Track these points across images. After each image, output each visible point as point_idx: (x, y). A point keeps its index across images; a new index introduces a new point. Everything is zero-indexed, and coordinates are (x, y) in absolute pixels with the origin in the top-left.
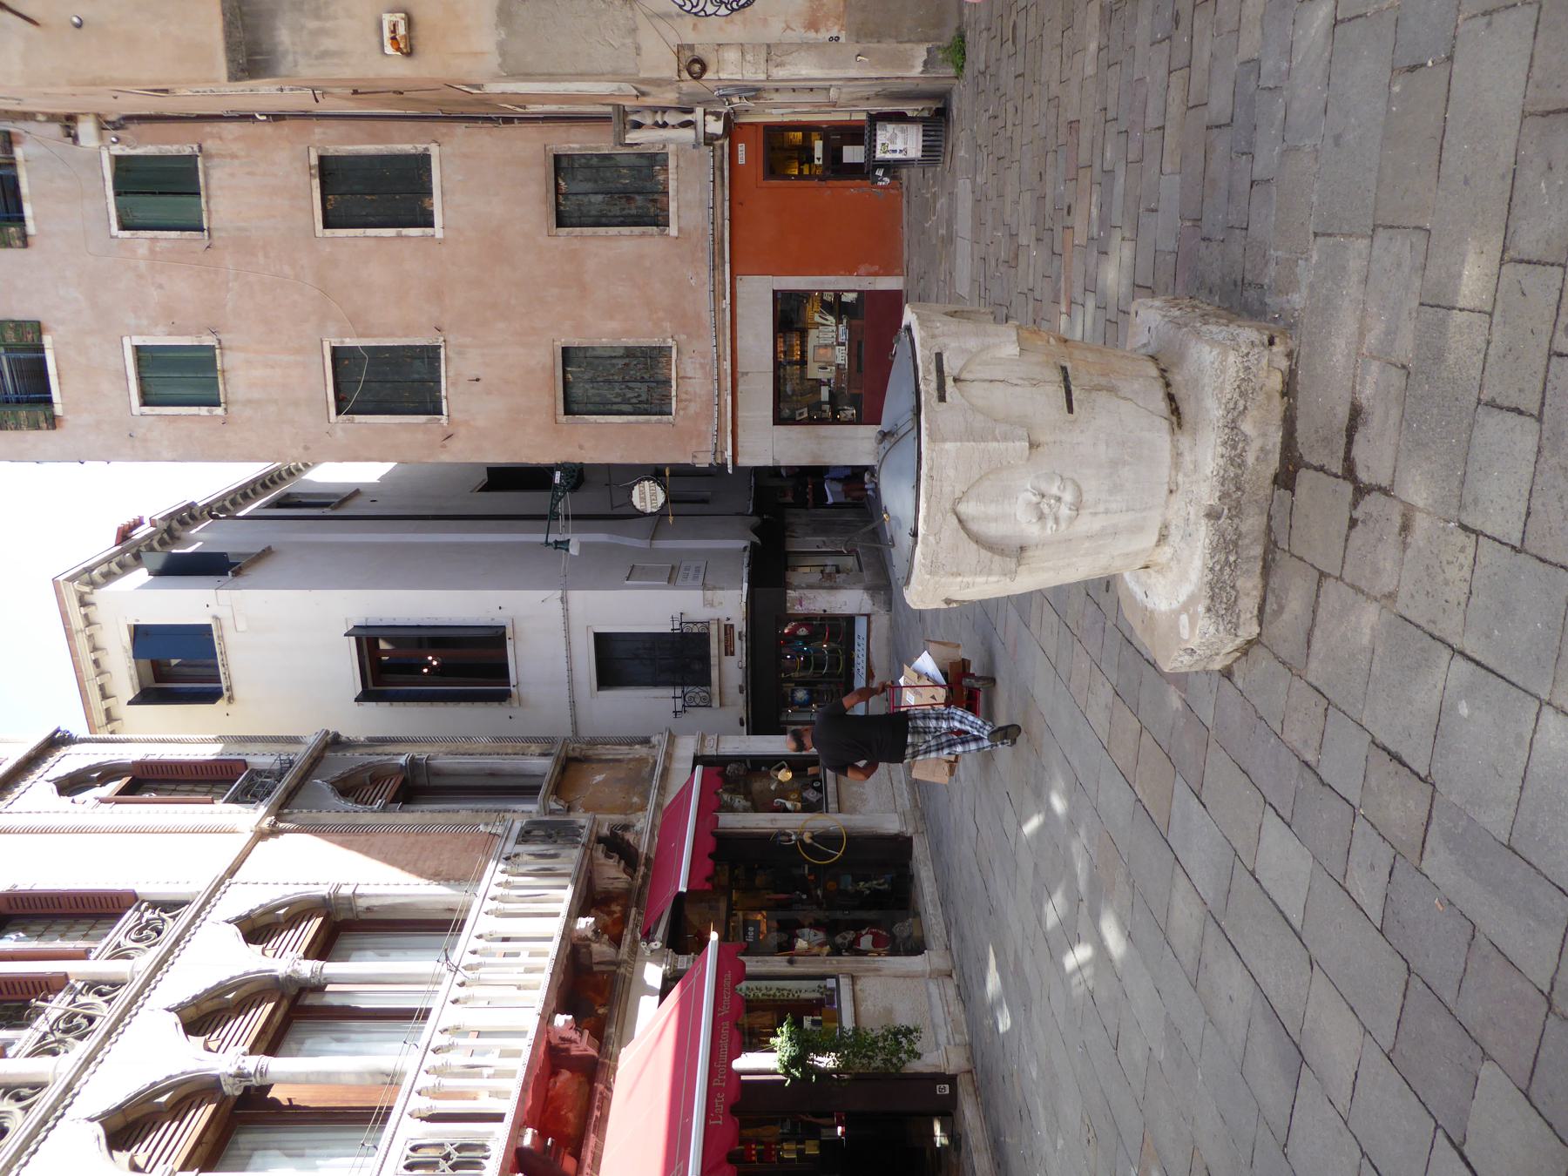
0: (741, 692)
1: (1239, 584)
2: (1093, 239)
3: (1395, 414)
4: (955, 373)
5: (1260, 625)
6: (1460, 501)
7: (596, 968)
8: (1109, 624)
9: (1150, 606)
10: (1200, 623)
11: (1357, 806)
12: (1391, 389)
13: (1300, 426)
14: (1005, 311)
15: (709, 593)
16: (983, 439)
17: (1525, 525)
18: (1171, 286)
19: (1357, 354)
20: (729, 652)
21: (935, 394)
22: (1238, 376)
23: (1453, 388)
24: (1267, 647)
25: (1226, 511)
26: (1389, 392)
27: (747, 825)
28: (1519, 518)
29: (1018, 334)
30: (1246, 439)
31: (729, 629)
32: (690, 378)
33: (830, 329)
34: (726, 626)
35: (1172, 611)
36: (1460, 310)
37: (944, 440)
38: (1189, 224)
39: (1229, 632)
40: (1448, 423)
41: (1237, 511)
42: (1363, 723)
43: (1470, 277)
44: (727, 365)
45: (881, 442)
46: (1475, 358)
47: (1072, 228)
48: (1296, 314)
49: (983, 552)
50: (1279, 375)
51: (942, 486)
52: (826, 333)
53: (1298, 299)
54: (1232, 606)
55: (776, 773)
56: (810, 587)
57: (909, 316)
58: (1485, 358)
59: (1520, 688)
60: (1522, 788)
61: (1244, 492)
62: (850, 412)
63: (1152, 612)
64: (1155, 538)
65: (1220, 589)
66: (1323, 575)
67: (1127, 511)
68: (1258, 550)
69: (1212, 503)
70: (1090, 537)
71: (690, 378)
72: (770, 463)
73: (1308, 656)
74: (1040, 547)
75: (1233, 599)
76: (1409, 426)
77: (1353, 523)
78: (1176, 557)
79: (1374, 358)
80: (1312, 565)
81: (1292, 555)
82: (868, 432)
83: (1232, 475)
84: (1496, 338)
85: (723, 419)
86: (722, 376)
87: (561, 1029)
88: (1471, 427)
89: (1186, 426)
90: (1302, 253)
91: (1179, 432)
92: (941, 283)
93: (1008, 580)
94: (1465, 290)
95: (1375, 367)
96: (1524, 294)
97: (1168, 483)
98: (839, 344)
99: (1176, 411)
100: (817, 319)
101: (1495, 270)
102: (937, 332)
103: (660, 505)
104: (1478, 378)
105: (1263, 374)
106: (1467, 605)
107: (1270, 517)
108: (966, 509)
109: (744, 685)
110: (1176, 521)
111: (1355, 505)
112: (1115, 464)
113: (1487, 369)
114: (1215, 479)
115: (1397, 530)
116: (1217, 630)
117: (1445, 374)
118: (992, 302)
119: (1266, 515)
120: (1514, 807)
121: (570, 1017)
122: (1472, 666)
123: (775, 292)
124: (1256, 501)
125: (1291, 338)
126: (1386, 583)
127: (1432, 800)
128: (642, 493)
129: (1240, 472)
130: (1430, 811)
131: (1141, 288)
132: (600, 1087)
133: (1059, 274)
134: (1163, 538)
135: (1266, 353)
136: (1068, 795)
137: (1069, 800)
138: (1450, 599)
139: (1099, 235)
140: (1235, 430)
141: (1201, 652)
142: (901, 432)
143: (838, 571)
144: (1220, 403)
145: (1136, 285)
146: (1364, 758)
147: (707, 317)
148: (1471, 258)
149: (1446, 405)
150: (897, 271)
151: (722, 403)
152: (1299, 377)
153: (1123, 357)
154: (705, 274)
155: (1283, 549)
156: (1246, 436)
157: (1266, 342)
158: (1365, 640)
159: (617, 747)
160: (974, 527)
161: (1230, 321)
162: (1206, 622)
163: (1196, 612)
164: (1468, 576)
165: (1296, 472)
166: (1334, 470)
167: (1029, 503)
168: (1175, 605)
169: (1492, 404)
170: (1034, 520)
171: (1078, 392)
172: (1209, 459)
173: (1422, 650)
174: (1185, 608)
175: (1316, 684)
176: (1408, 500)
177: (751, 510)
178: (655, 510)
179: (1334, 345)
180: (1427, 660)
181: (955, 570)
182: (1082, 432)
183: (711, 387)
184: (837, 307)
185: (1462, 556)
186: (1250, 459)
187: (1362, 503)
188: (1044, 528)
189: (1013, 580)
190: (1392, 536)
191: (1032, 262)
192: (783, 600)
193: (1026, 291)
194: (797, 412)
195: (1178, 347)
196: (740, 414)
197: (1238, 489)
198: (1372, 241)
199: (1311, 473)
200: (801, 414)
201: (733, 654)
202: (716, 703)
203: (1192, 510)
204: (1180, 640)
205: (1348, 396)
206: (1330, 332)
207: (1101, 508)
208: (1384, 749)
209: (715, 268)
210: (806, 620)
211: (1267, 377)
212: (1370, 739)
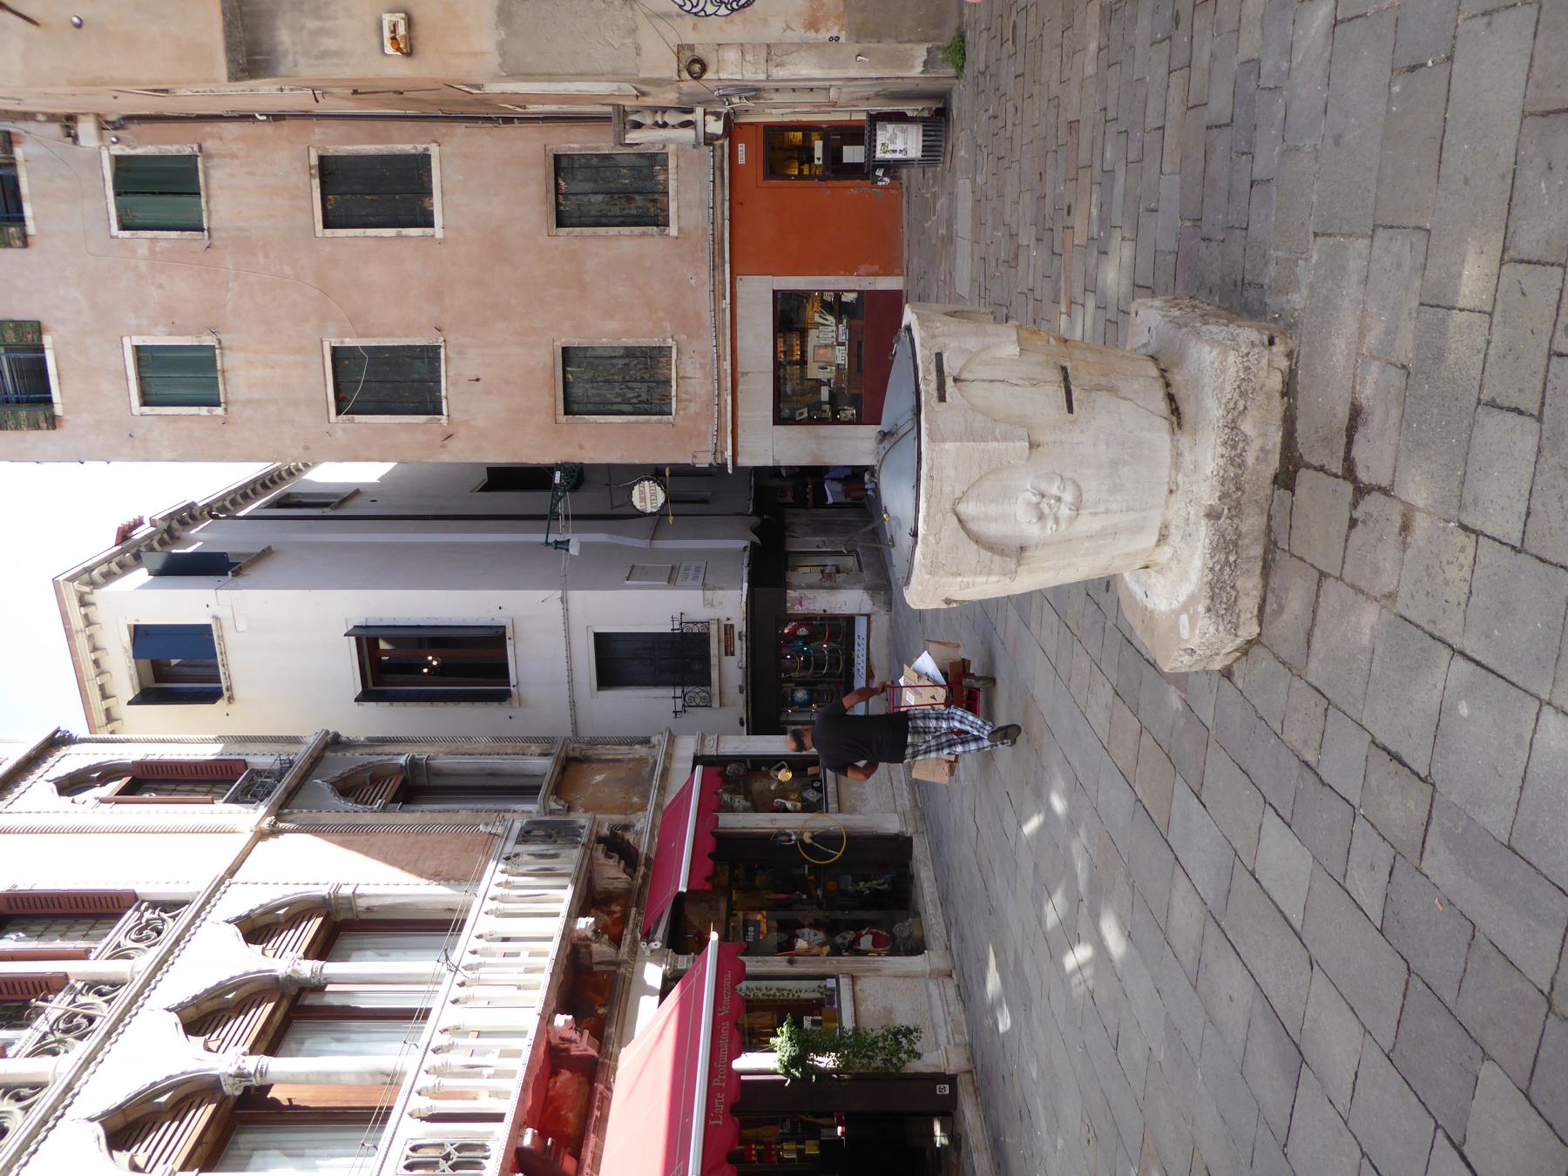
0: (741, 692)
1: (1239, 584)
2: (1093, 239)
3: (1395, 414)
4: (955, 373)
5: (1260, 625)
6: (1460, 501)
7: (596, 968)
8: (1109, 624)
9: (1150, 606)
10: (1200, 623)
11: (1357, 806)
12: (1391, 389)
13: (1300, 426)
14: (1005, 311)
15: (709, 593)
16: (983, 439)
17: (1525, 525)
18: (1171, 286)
19: (1357, 354)
20: (729, 652)
21: (935, 394)
22: (1238, 376)
23: (1453, 388)
24: (1267, 647)
25: (1226, 511)
26: (1389, 392)
27: (747, 825)
28: (1519, 518)
29: (1018, 334)
30: (1246, 439)
31: (729, 629)
32: (690, 378)
33: (830, 329)
34: (726, 626)
35: (1172, 611)
36: (1460, 310)
37: (944, 440)
38: (1189, 224)
39: (1229, 632)
40: (1448, 423)
41: (1237, 511)
42: (1363, 723)
43: (1470, 277)
44: (727, 365)
45: (881, 442)
46: (1475, 358)
47: (1072, 228)
48: (1296, 314)
49: (983, 552)
50: (1279, 375)
51: (942, 486)
52: (826, 333)
53: (1298, 299)
54: (1232, 606)
55: (776, 773)
56: (810, 587)
57: (909, 316)
58: (1485, 358)
59: (1520, 688)
60: (1522, 788)
61: (1244, 492)
62: (850, 412)
63: (1152, 612)
64: (1155, 538)
65: (1220, 589)
66: (1323, 575)
67: (1127, 511)
68: (1258, 550)
69: (1212, 503)
70: (1090, 537)
71: (690, 378)
72: (770, 463)
73: (1308, 656)
74: (1040, 547)
75: (1233, 599)
76: (1409, 426)
77: (1353, 523)
78: (1176, 557)
79: (1374, 358)
80: (1312, 565)
81: (1292, 555)
82: (868, 432)
83: (1232, 475)
84: (1496, 338)
85: (723, 419)
86: (722, 376)
87: (561, 1029)
88: (1471, 427)
89: (1186, 426)
90: (1302, 253)
91: (1179, 432)
92: (941, 283)
93: (1008, 580)
94: (1465, 290)
95: (1375, 367)
96: (1524, 294)
97: (1168, 483)
98: (839, 344)
99: (1176, 411)
100: (817, 319)
101: (1495, 270)
102: (937, 332)
103: (660, 505)
104: (1478, 378)
105: (1263, 374)
106: (1467, 605)
107: (1270, 517)
108: (966, 509)
109: (744, 685)
110: (1176, 521)
111: (1355, 505)
112: (1115, 464)
113: (1487, 369)
114: (1215, 479)
115: (1397, 530)
116: (1217, 630)
117: (1445, 374)
118: (992, 302)
119: (1266, 515)
120: (1514, 807)
121: (570, 1017)
122: (1472, 666)
123: (775, 292)
124: (1256, 501)
125: (1291, 338)
126: (1386, 583)
127: (1432, 800)
128: (642, 493)
129: (1240, 472)
130: (1430, 811)
131: (1141, 288)
132: (600, 1087)
133: (1059, 274)
134: (1163, 538)
135: (1266, 353)
136: (1068, 795)
137: (1069, 800)
138: (1450, 599)
139: (1099, 235)
140: (1235, 430)
141: (1201, 652)
142: (901, 432)
143: (838, 571)
144: (1220, 403)
145: (1136, 285)
146: (1364, 758)
147: (707, 317)
148: (1471, 258)
149: (1446, 405)
150: (897, 271)
151: (722, 403)
152: (1299, 377)
153: (1123, 357)
154: (705, 274)
155: (1283, 549)
156: (1246, 436)
157: (1266, 342)
158: (1365, 640)
159: (617, 747)
160: (974, 527)
161: (1230, 321)
162: (1206, 622)
163: (1196, 612)
164: (1468, 576)
165: (1296, 472)
166: (1334, 470)
167: (1029, 503)
168: (1175, 605)
169: (1492, 404)
170: (1034, 520)
171: (1078, 392)
172: (1209, 459)
173: (1422, 650)
174: (1185, 608)
175: (1316, 684)
176: (1408, 500)
177: (751, 510)
178: (655, 510)
179: (1334, 345)
180: (1427, 660)
181: (955, 570)
182: (1082, 432)
183: (711, 387)
184: (837, 307)
185: (1462, 556)
186: (1250, 459)
187: (1362, 503)
188: (1044, 528)
189: (1013, 580)
190: (1392, 536)
191: (1032, 262)
192: (783, 600)
193: (1026, 291)
194: (797, 412)
195: (1178, 347)
196: (740, 414)
197: (1238, 489)
198: (1372, 241)
199: (1311, 473)
200: (801, 414)
201: (733, 654)
202: (716, 703)
203: (1192, 510)
204: (1180, 640)
205: (1348, 396)
206: (1330, 332)
207: (1101, 508)
208: (1384, 749)
209: (715, 268)
210: (806, 620)
211: (1267, 377)
212: (1370, 739)
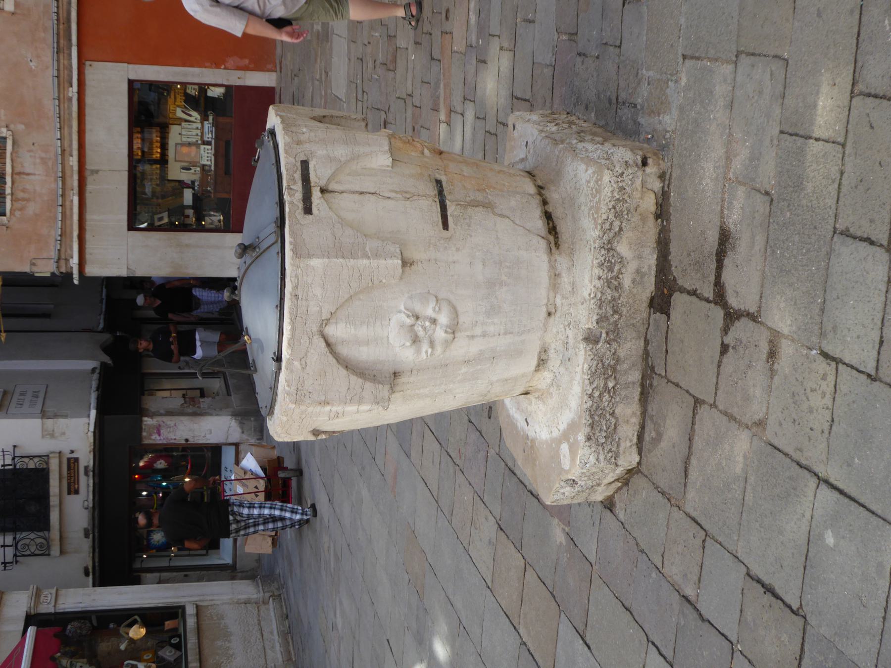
0: (87, 536)
1: (618, 411)
2: (471, 46)
3: (760, 239)
4: (323, 183)
5: (640, 454)
6: (821, 328)
8: (492, 452)
9: (531, 434)
10: (580, 452)
11: (735, 642)
12: (756, 215)
13: (674, 248)
14: (383, 116)
15: (49, 423)
16: (353, 256)
17: (879, 353)
18: (549, 100)
19: (725, 178)
20: (73, 489)
21: (301, 205)
22: (613, 197)
23: (812, 216)
24: (647, 477)
25: (604, 335)
26: (754, 218)
28: (874, 347)
29: (390, 143)
30: (622, 260)
31: (73, 463)
32: (28, 174)
33: (194, 125)
34: (69, 459)
35: (553, 440)
36: (817, 140)
37: (310, 256)
38: (565, 37)
39: (609, 461)
40: (808, 251)
41: (615, 335)
42: (739, 555)
43: (824, 107)
44: (74, 161)
45: (657, 220)
46: (830, 187)
47: (451, 33)
48: (668, 135)
49: (354, 379)
50: (653, 196)
51: (308, 306)
52: (189, 130)
53: (669, 120)
54: (611, 434)
55: (126, 630)
56: (170, 413)
57: (273, 120)
58: (839, 188)
59: (880, 517)
60: (884, 618)
61: (621, 315)
62: (217, 218)
63: (533, 441)
64: (534, 363)
65: (600, 416)
66: (698, 402)
67: (505, 334)
68: (635, 376)
69: (590, 326)
70: (467, 362)
71: (28, 174)
72: (124, 273)
73: (685, 486)
74: (415, 372)
75: (613, 427)
76: (774, 252)
77: (724, 349)
78: (555, 383)
79: (739, 183)
80: (687, 392)
81: (669, 381)
82: (233, 240)
83: (609, 298)
84: (848, 168)
85: (68, 222)
86: (68, 173)
88: (829, 255)
89: (564, 246)
90: (672, 75)
91: (557, 252)
92: (317, 83)
93: (381, 408)
94: (820, 121)
95: (741, 192)
96: (872, 127)
97: (547, 305)
98: (205, 143)
99: (553, 230)
100: (179, 113)
101: (846, 102)
102: (302, 138)
104: (834, 207)
105: (637, 195)
106: (830, 433)
107: (647, 342)
108: (336, 331)
110: (555, 345)
111: (726, 330)
112: (492, 284)
113: (842, 200)
114: (592, 301)
115: (765, 356)
116: (598, 460)
117: (804, 202)
118: (370, 107)
119: (643, 339)
120: (878, 638)
122: (836, 495)
123: (131, 83)
124: (633, 325)
125: (663, 159)
126: (756, 411)
127: (804, 633)
129: (617, 295)
130: (803, 645)
131: (518, 101)
133: (439, 80)
134: (542, 363)
135: (640, 173)
136: (452, 641)
137: (453, 647)
138: (814, 427)
139: (478, 42)
140: (612, 252)
141: (583, 484)
142: (264, 245)
143: (203, 395)
144: (596, 224)
145: (514, 97)
146: (740, 591)
147: (50, 106)
148: (825, 89)
149: (806, 233)
150: (270, 66)
151: (68, 203)
152: (672, 199)
153: (500, 172)
154: (48, 56)
155: (660, 375)
156: (622, 258)
157: (640, 162)
158: (738, 469)
160: (343, 351)
161: (606, 140)
162: (587, 451)
163: (576, 440)
164: (830, 404)
165: (671, 296)
166: (706, 295)
167: (402, 326)
168: (556, 434)
169: (846, 233)
170: (408, 344)
171: (453, 207)
172: (587, 281)
173: (791, 478)
174: (565, 436)
175: (694, 514)
176: (774, 327)
177: (101, 326)
179: (703, 168)
180: (795, 489)
181: (323, 398)
182: (458, 250)
183: (53, 186)
184: (202, 101)
185: (824, 384)
186: (627, 281)
187: (733, 328)
188: (418, 352)
189: (386, 408)
190: (760, 364)
191: (410, 66)
193: (405, 97)
194: (156, 217)
195: (554, 164)
196: (89, 216)
197: (615, 312)
198: (736, 67)
199: (685, 297)
200: (161, 219)
201: (77, 492)
202: (55, 550)
203: (570, 333)
204: (562, 471)
205: (717, 221)
206: (699, 155)
207: (478, 331)
208: (759, 581)
209: (60, 51)
210: (166, 451)
211: (642, 198)
212: (744, 570)
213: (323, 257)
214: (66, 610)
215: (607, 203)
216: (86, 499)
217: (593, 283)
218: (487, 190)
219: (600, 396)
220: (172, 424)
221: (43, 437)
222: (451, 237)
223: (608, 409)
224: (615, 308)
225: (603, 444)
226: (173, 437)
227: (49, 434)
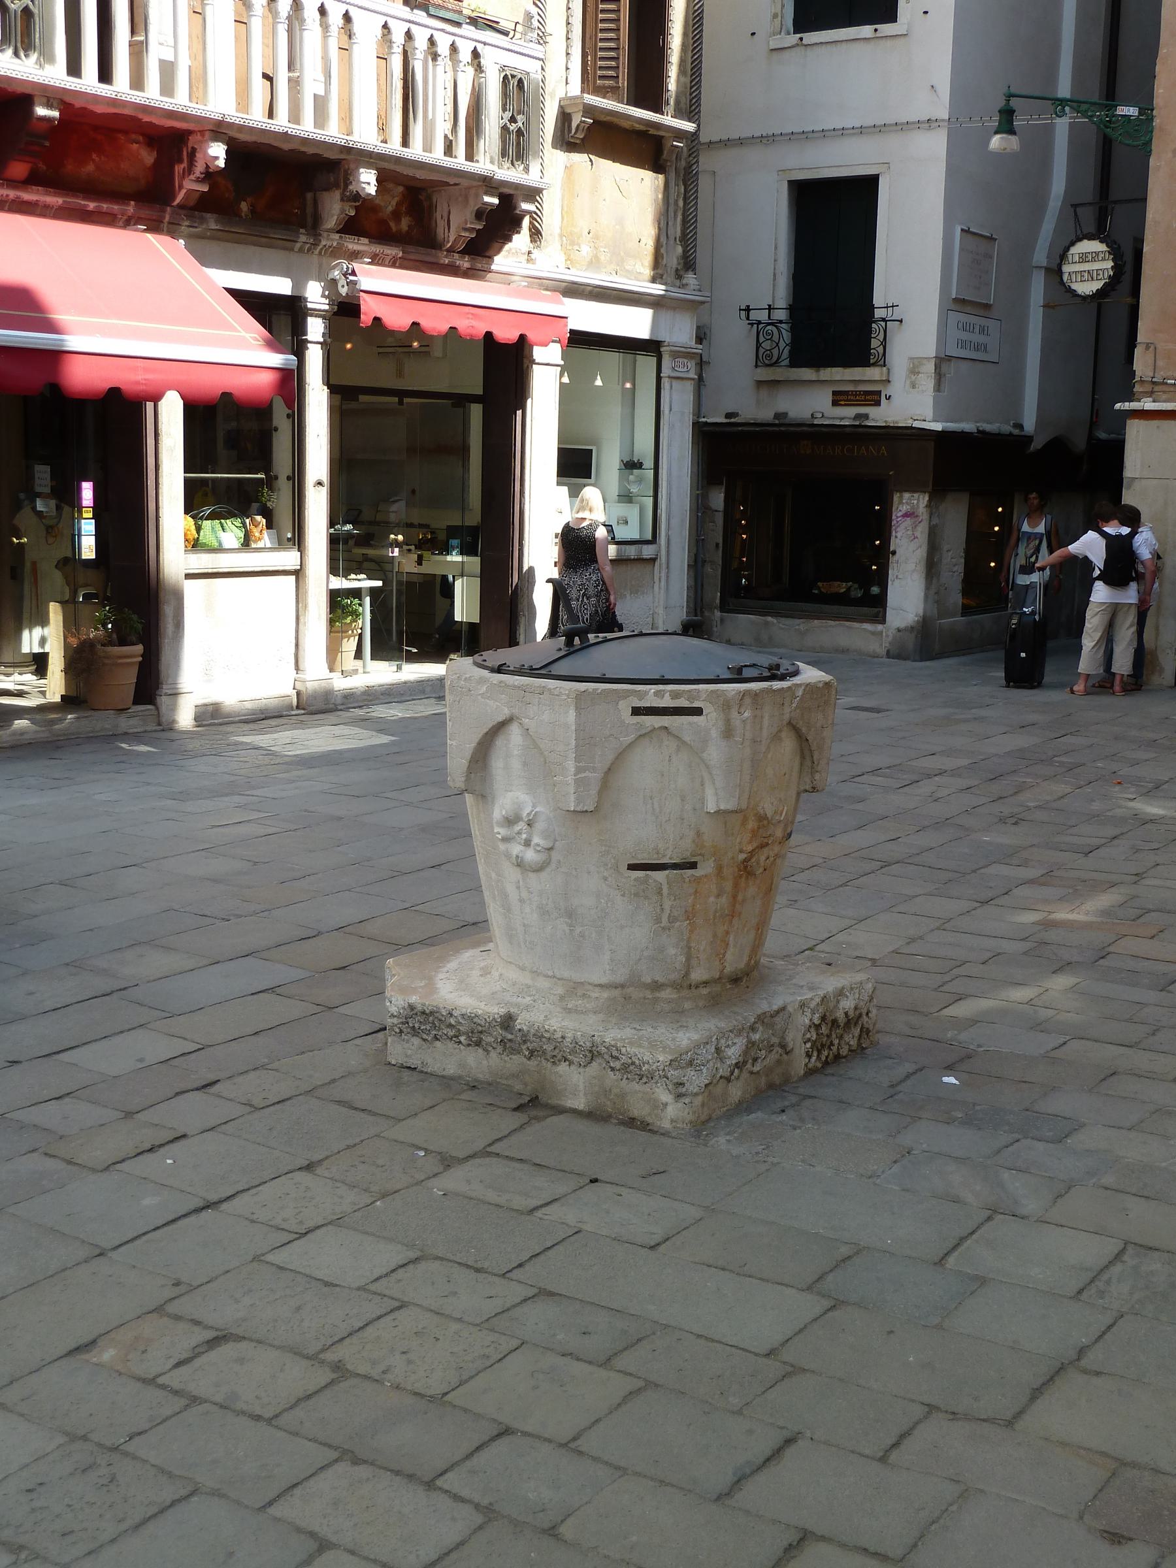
0: (777, 416)
7: (309, 196)
15: (930, 367)
20: (839, 398)
22: (644, 1063)
25: (510, 1036)
31: (873, 398)
34: (879, 393)
37: (578, 709)
61: (529, 1059)
72: (1128, 473)
87: (206, 153)
103: (1074, 286)
109: (787, 421)
112: (570, 914)
128: (1095, 256)
132: (131, 208)
159: (680, 217)
178: (1065, 278)
188: (500, 825)
192: (914, 487)
201: (835, 403)
202: (764, 374)
213: (578, 725)
214: (662, 390)
215: (636, 1055)
216: (825, 415)
217: (558, 1030)
218: (688, 922)
219: (450, 1026)
220: (918, 534)
221: (911, 359)
222: (619, 872)
223: (440, 1033)
224: (536, 1053)
225: (408, 1023)
226: (899, 535)
227: (914, 367)
